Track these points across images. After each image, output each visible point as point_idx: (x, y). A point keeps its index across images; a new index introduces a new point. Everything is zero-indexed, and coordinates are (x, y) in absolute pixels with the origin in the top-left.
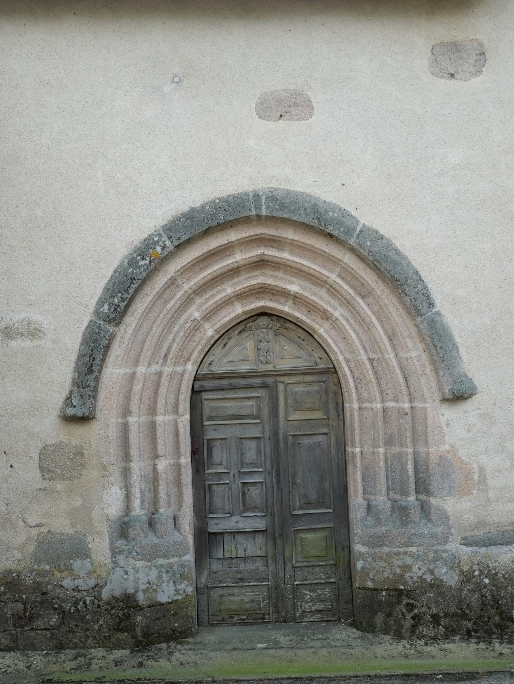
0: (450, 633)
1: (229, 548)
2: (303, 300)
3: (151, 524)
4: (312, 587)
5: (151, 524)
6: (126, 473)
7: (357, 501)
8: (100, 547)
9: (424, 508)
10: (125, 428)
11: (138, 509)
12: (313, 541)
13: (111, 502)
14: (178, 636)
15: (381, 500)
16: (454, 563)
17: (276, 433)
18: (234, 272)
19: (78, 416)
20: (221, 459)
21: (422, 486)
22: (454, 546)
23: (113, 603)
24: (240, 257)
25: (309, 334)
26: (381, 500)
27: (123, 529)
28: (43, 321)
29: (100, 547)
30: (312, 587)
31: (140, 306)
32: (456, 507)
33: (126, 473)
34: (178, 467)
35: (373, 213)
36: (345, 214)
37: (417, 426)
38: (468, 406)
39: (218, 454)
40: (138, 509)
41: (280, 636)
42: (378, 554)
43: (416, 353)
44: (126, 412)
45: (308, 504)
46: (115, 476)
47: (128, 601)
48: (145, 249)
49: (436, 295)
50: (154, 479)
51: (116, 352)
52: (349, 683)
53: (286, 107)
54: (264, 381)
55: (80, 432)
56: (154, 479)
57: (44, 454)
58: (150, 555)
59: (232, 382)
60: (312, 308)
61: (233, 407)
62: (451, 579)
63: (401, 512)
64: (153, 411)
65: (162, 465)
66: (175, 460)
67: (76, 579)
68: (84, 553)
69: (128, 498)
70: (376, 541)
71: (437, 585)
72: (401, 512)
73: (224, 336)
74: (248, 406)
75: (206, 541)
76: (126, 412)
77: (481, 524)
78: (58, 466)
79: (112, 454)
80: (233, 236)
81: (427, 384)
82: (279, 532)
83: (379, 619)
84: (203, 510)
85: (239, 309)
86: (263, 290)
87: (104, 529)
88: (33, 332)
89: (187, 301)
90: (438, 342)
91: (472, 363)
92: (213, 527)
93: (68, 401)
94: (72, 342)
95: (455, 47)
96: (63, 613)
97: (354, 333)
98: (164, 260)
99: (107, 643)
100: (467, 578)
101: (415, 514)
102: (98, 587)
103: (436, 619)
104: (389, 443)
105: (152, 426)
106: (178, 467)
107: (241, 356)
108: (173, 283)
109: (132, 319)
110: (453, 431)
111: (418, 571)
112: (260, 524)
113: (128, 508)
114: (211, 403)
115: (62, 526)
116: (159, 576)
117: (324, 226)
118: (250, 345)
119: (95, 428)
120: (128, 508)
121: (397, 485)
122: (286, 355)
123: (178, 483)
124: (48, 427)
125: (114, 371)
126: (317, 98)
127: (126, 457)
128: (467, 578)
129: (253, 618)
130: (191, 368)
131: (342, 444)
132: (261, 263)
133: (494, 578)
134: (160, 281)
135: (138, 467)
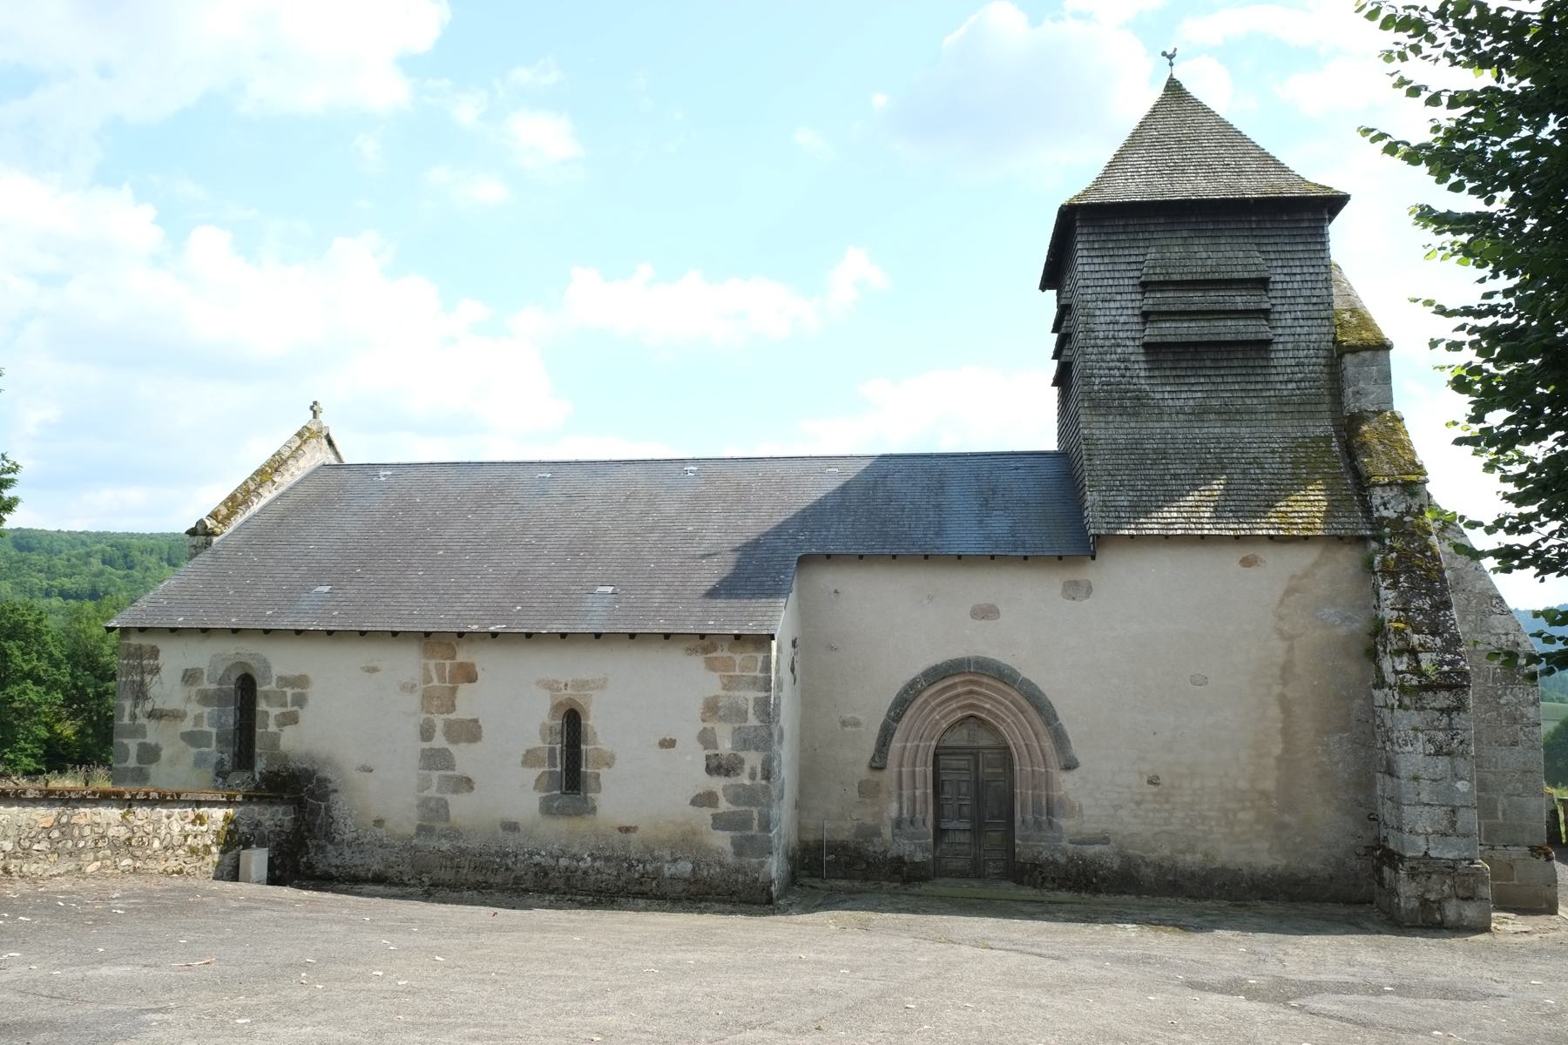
0: (1060, 888)
1: (951, 838)
2: (902, 756)
3: (912, 822)
4: (994, 861)
5: (912, 822)
6: (900, 796)
7: (1018, 817)
8: (887, 832)
9: (1050, 823)
10: (900, 773)
11: (905, 814)
12: (995, 837)
13: (893, 810)
14: (925, 879)
15: (1029, 817)
16: (1064, 852)
17: (977, 778)
18: (958, 696)
19: (878, 763)
20: (948, 790)
21: (1050, 812)
22: (1065, 843)
23: (893, 860)
24: (960, 690)
25: (996, 729)
26: (1029, 817)
27: (898, 824)
28: (862, 718)
29: (887, 832)
30: (994, 861)
31: (909, 713)
32: (1067, 824)
33: (900, 796)
34: (926, 794)
35: (1028, 672)
36: (1014, 671)
37: (1048, 782)
38: (1074, 772)
39: (947, 788)
40: (905, 814)
41: (976, 883)
42: (1027, 846)
43: (1048, 744)
44: (901, 765)
45: (993, 817)
46: (895, 798)
47: (900, 859)
48: (912, 685)
49: (1060, 714)
50: (914, 800)
51: (897, 735)
52: (634, 1041)
53: (986, 613)
54: (974, 753)
55: (877, 774)
56: (914, 800)
57: (860, 784)
58: (911, 837)
59: (955, 751)
60: (997, 716)
61: (955, 764)
62: (1062, 860)
63: (1038, 823)
64: (914, 765)
65: (918, 793)
66: (924, 790)
67: (875, 847)
68: (879, 834)
69: (901, 808)
70: (1025, 839)
71: (1055, 863)
72: (1038, 823)
73: (951, 727)
74: (963, 764)
75: (939, 833)
76: (901, 765)
77: (1079, 833)
78: (868, 791)
79: (893, 787)
80: (957, 679)
81: (1053, 759)
82: (978, 830)
83: (1026, 878)
84: (938, 816)
85: (959, 715)
86: (971, 706)
87: (889, 823)
88: (857, 724)
89: (933, 709)
90: (1060, 738)
91: (1077, 750)
92: (943, 826)
93: (873, 759)
94: (875, 730)
95: (1076, 583)
96: (868, 863)
97: (1017, 730)
98: (920, 692)
99: (889, 879)
100: (1071, 860)
101: (1045, 826)
102: (885, 852)
103: (1053, 880)
104: (1034, 788)
105: (914, 772)
106: (926, 794)
107: (960, 738)
108: (926, 702)
109: (905, 719)
110: (1067, 785)
111: (1046, 854)
112: (968, 826)
113: (901, 813)
114: (943, 760)
115: (869, 821)
116: (915, 848)
117: (1003, 675)
118: (965, 732)
119: (886, 772)
120: (901, 813)
121: (1037, 810)
122: (984, 740)
123: (926, 802)
124: (863, 771)
125: (896, 745)
126: (1002, 609)
127: (900, 788)
128: (1071, 860)
129: (963, 875)
130: (934, 743)
131: (1012, 786)
132: (971, 692)
133: (1084, 861)
134: (920, 701)
135: (906, 793)
